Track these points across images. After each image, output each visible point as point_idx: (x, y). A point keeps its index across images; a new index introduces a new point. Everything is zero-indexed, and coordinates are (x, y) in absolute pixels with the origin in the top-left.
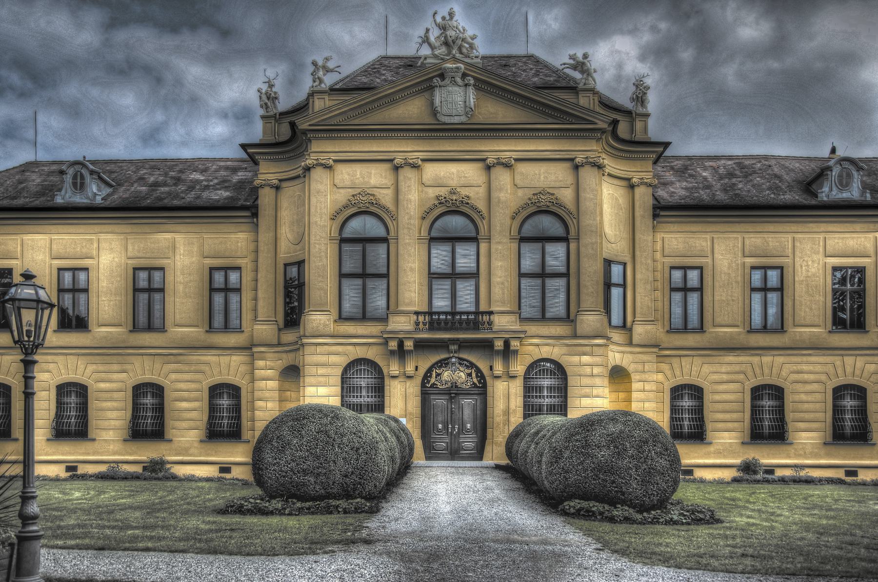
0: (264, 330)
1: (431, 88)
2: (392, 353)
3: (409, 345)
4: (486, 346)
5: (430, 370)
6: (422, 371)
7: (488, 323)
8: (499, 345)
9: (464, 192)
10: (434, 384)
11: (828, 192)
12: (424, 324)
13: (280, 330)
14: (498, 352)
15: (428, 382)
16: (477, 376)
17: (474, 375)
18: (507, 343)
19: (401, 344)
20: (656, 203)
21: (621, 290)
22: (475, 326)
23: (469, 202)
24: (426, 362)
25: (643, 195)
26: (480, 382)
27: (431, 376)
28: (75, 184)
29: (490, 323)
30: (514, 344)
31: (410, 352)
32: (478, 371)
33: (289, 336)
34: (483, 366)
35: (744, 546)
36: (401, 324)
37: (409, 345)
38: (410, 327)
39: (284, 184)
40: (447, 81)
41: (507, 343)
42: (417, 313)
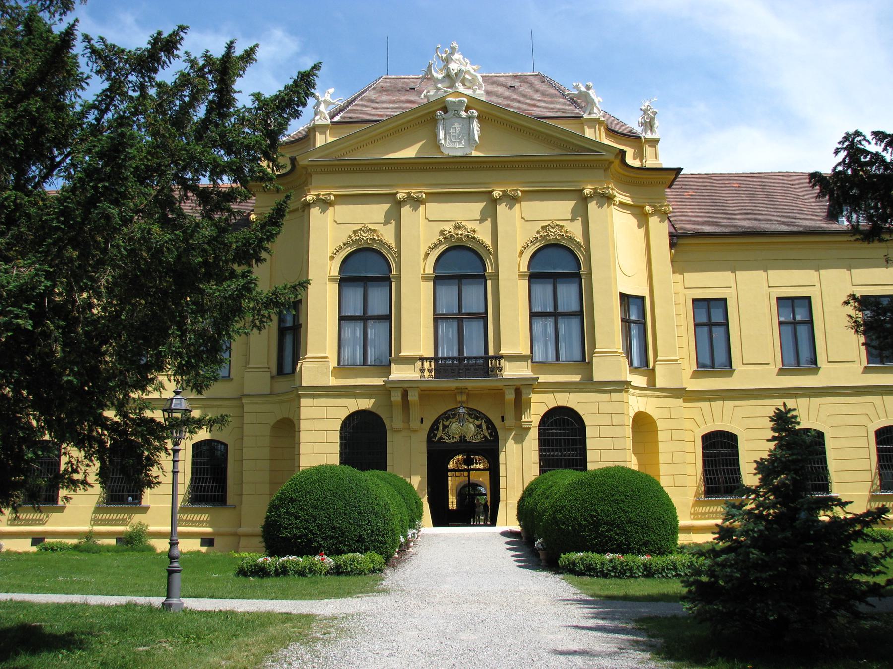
5: (435, 424)
6: (427, 425)
7: (428, 370)
10: (441, 438)
12: (430, 371)
13: (272, 377)
15: (435, 435)
16: (488, 428)
17: (484, 427)
20: (673, 231)
23: (476, 236)
26: (490, 434)
27: (437, 429)
32: (489, 422)
40: (451, 114)
42: (422, 359)
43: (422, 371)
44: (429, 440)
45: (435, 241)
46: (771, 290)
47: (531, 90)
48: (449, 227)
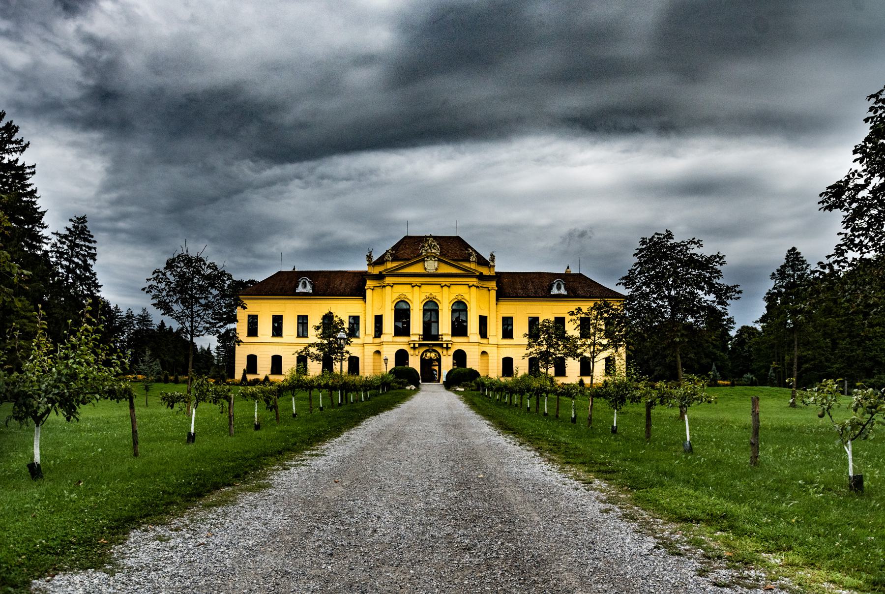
0: (370, 339)
1: (424, 261)
2: (411, 348)
3: (417, 345)
4: (441, 345)
6: (421, 353)
8: (445, 346)
9: (434, 294)
14: (445, 348)
21: (436, 324)
22: (437, 339)
24: (422, 350)
29: (442, 338)
30: (450, 345)
31: (417, 348)
33: (377, 340)
34: (440, 351)
35: (709, 558)
36: (614, 351)
37: (417, 345)
39: (423, 286)
42: (420, 335)
48: (428, 294)
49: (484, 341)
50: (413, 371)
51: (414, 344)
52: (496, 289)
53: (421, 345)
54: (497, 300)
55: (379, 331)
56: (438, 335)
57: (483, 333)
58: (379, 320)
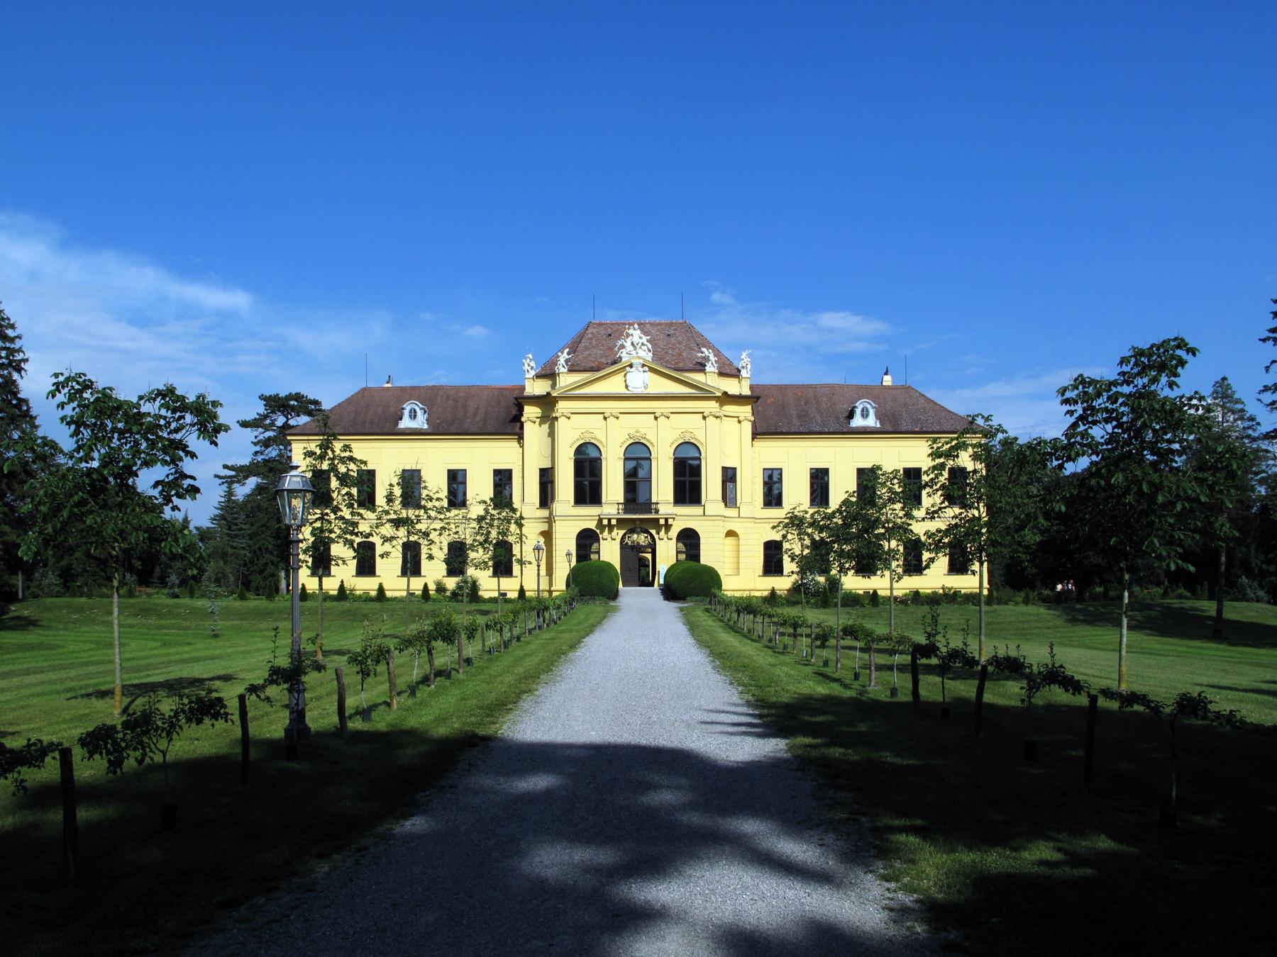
3: (614, 522)
8: (662, 522)
9: (643, 431)
11: (857, 422)
18: (666, 520)
19: (609, 520)
25: (747, 427)
28: (410, 416)
30: (670, 521)
38: (616, 512)
41: (666, 520)
42: (618, 504)
43: (618, 510)
44: (621, 543)
45: (624, 439)
46: (901, 464)
47: (680, 338)
48: (632, 432)
49: (732, 512)
50: (609, 566)
51: (609, 520)
52: (753, 419)
53: (618, 520)
54: (753, 439)
55: (547, 496)
56: (651, 503)
57: (728, 498)
58: (547, 479)
